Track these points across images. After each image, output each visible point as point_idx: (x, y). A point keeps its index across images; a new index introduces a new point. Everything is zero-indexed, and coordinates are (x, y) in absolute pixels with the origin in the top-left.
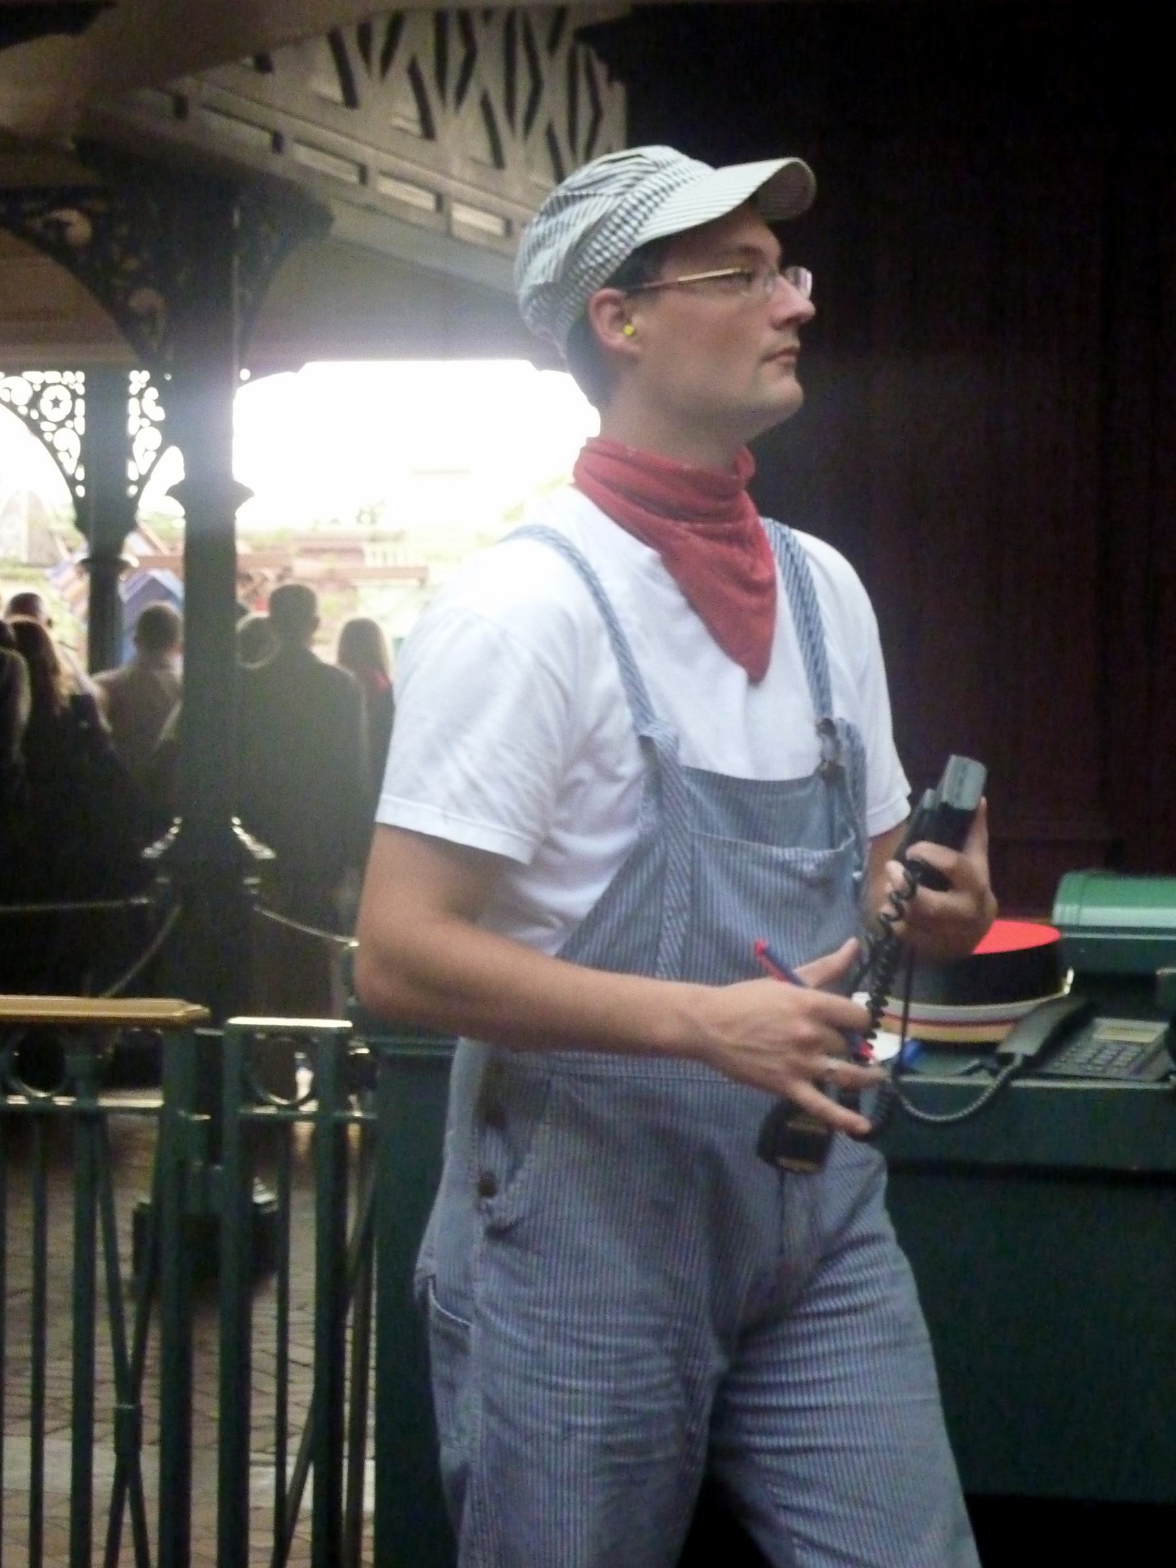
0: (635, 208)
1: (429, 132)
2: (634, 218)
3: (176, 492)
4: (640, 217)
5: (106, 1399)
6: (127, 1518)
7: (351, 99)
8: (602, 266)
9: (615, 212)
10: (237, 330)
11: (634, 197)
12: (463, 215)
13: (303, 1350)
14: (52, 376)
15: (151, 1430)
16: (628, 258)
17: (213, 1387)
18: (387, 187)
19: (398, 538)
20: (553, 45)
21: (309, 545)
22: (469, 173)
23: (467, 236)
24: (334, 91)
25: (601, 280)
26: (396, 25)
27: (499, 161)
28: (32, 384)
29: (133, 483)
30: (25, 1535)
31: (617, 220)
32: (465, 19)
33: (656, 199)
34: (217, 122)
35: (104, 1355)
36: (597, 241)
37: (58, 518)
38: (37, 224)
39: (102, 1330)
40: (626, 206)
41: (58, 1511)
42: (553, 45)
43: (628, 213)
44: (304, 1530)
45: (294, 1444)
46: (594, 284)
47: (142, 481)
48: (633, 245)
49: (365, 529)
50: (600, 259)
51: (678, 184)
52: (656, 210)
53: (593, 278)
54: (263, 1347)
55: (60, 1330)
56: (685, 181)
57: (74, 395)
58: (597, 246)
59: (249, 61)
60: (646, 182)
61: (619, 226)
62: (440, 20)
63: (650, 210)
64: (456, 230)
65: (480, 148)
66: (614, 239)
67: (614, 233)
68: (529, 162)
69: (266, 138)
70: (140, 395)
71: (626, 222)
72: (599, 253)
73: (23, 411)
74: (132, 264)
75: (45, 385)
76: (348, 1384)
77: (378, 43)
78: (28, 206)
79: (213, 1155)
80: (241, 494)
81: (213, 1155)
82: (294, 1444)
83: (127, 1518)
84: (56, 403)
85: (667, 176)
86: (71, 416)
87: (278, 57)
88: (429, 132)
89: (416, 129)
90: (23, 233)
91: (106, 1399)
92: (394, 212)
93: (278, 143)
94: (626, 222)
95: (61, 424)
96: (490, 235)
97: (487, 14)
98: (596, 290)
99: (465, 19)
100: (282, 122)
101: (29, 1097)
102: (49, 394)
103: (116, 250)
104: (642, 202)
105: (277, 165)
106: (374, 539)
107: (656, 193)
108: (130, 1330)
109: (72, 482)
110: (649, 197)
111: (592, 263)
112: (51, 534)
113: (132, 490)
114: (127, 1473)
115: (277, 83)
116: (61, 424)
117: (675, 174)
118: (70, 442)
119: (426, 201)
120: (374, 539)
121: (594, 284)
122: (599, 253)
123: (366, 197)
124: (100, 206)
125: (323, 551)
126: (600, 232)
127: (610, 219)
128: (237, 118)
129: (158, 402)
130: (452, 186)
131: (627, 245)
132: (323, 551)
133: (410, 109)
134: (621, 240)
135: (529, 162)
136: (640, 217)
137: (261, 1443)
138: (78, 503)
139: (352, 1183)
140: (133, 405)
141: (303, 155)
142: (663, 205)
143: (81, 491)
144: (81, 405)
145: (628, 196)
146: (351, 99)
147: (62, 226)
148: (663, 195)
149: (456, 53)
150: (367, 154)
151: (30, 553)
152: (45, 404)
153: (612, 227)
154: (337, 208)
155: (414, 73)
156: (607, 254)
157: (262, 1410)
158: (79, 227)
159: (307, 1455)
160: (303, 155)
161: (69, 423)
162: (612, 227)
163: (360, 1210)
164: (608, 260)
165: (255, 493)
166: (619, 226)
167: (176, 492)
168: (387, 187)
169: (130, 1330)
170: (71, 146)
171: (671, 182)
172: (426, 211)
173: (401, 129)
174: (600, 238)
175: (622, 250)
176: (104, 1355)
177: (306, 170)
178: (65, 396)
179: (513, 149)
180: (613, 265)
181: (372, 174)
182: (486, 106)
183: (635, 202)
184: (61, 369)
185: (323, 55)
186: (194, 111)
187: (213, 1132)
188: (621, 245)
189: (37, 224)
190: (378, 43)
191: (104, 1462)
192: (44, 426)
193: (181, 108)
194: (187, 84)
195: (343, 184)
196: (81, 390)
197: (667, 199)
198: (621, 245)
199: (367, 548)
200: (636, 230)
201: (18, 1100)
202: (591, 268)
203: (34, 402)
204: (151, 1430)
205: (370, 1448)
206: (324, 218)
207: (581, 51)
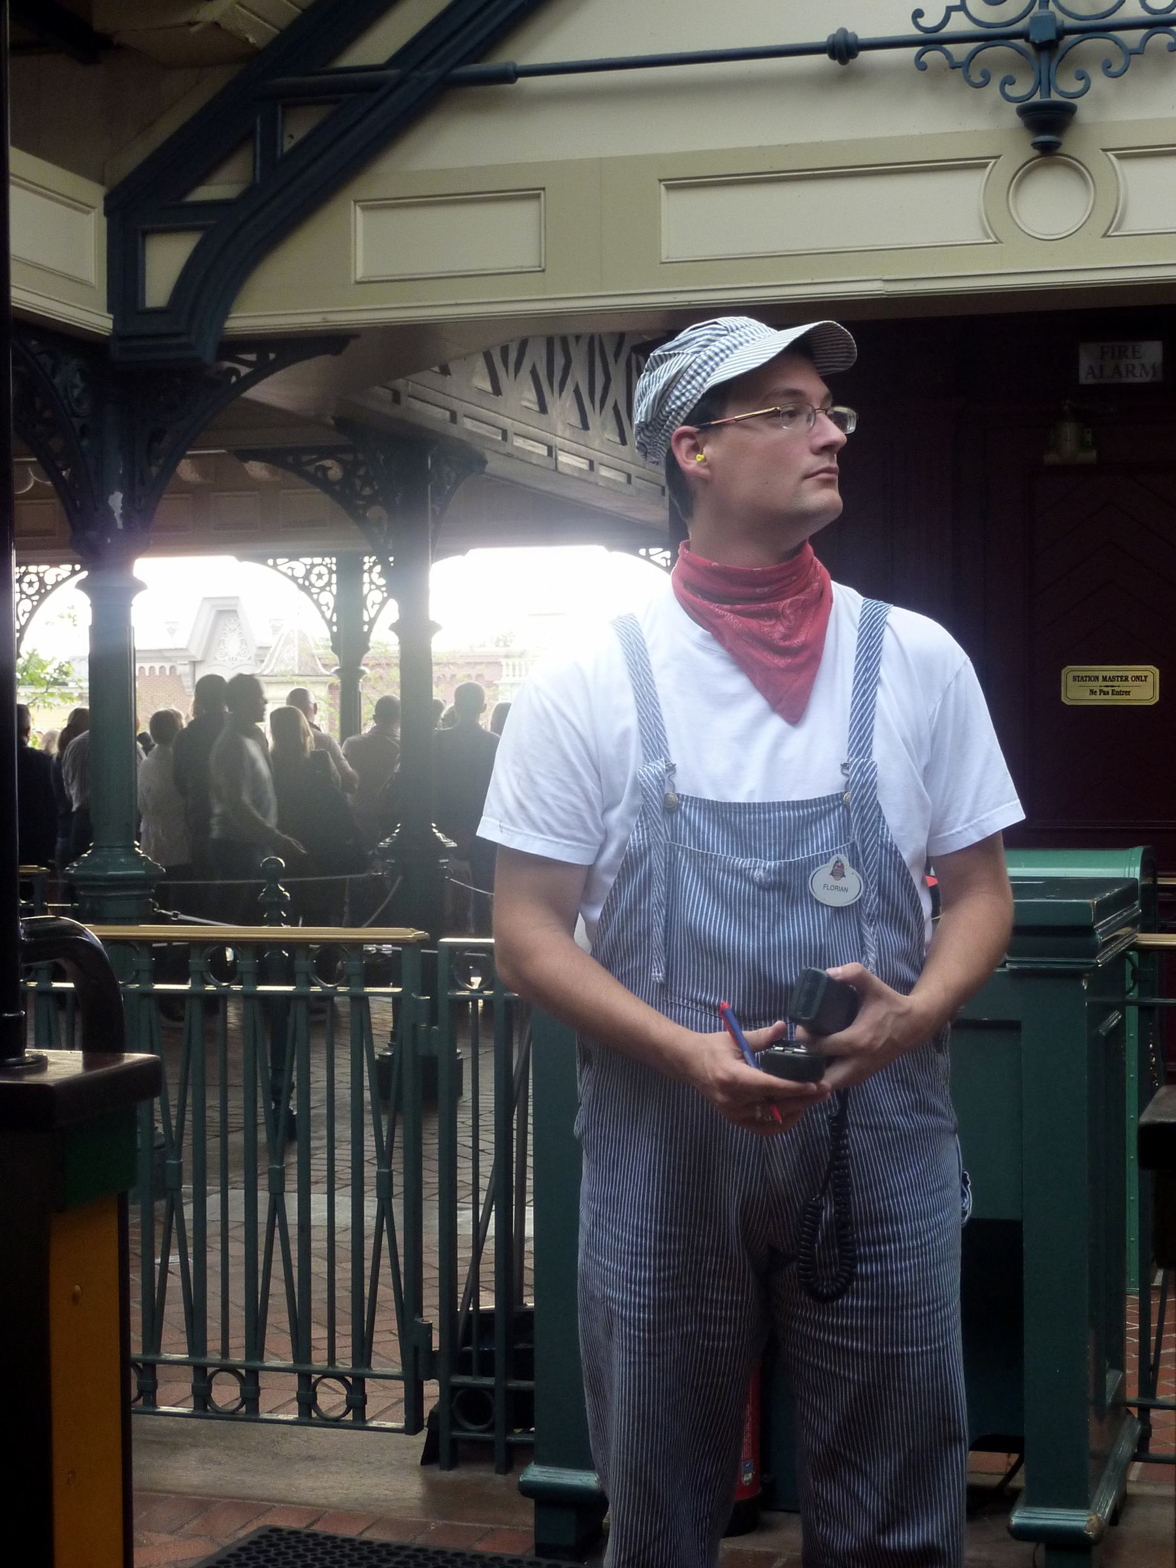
0: (706, 363)
1: (543, 409)
2: (705, 370)
3: (395, 628)
4: (708, 369)
5: (370, 1172)
6: (385, 1241)
7: (497, 391)
8: (681, 408)
9: (690, 366)
10: (431, 527)
11: (705, 354)
12: (563, 458)
13: (488, 1141)
14: (317, 560)
15: (398, 1189)
16: (700, 401)
17: (435, 1165)
18: (519, 442)
19: (522, 655)
20: (617, 355)
21: (468, 660)
22: (567, 434)
23: (567, 471)
24: (488, 387)
25: (682, 420)
26: (523, 345)
27: (585, 426)
28: (306, 565)
29: (366, 623)
30: (325, 1253)
31: (691, 373)
32: (564, 340)
33: (722, 355)
34: (418, 405)
35: (370, 1144)
36: (678, 389)
37: (317, 646)
38: (311, 469)
39: (369, 1133)
40: (699, 361)
41: (344, 1239)
42: (617, 355)
43: (700, 367)
44: (489, 1247)
45: (483, 1196)
46: (676, 422)
47: (372, 622)
48: (703, 391)
49: (502, 650)
50: (679, 403)
51: (741, 344)
52: (726, 360)
53: (675, 418)
54: (464, 1139)
55: (344, 1130)
56: (747, 342)
57: (331, 572)
58: (677, 393)
59: (436, 369)
60: (717, 343)
61: (693, 377)
62: (550, 341)
63: (722, 360)
64: (560, 468)
65: (575, 419)
66: (689, 387)
67: (689, 383)
68: (604, 427)
69: (448, 414)
70: (371, 569)
71: (699, 374)
72: (678, 398)
73: (301, 581)
74: (367, 491)
75: (313, 566)
76: (515, 1154)
77: (513, 356)
78: (305, 458)
79: (433, 1020)
80: (434, 628)
81: (433, 1020)
82: (483, 1196)
83: (385, 1241)
84: (320, 576)
85: (734, 337)
86: (329, 584)
87: (452, 367)
88: (543, 409)
89: (536, 407)
90: (303, 474)
91: (370, 1172)
92: (522, 458)
93: (454, 417)
94: (699, 374)
95: (322, 589)
96: (580, 469)
97: (578, 338)
98: (677, 426)
99: (564, 340)
100: (456, 405)
101: (322, 987)
102: (316, 570)
103: (358, 482)
104: (711, 358)
105: (454, 431)
106: (507, 656)
107: (722, 351)
108: (385, 1129)
109: (330, 623)
110: (717, 354)
111: (673, 407)
112: (313, 656)
113: (366, 628)
114: (385, 1211)
115: (452, 383)
116: (322, 589)
117: (741, 336)
118: (328, 598)
119: (543, 451)
120: (507, 656)
121: (676, 422)
122: (678, 398)
123: (508, 449)
124: (349, 457)
125: (276, 683)
126: (679, 382)
127: (686, 371)
128: (427, 402)
129: (381, 574)
130: (558, 441)
131: (699, 391)
132: (276, 683)
133: (532, 395)
134: (694, 388)
135: (604, 427)
136: (708, 369)
137: (464, 1196)
138: (334, 637)
139: (516, 1039)
140: (366, 577)
141: (469, 424)
142: (726, 360)
143: (335, 629)
144: (334, 577)
145: (702, 353)
146: (497, 391)
147: (325, 469)
148: (728, 352)
149: (559, 361)
150: (507, 423)
151: (299, 669)
152: (313, 578)
153: (688, 378)
154: (489, 456)
155: (534, 374)
156: (684, 399)
157: (464, 1175)
158: (335, 472)
159: (492, 1198)
160: (469, 424)
161: (328, 588)
162: (688, 378)
163: (520, 1052)
164: (684, 404)
165: (146, 583)
166: (693, 377)
167: (395, 628)
168: (519, 442)
169: (385, 1129)
170: (332, 422)
171: (736, 343)
172: (543, 456)
173: (526, 407)
174: (680, 387)
175: (695, 396)
176: (370, 1144)
177: (470, 433)
178: (324, 571)
179: (594, 419)
180: (688, 407)
181: (510, 434)
182: (577, 392)
183: (705, 358)
184: (323, 555)
185: (480, 364)
186: (404, 399)
187: (433, 1003)
188: (694, 392)
189: (311, 469)
190: (513, 356)
191: (371, 1208)
192: (314, 590)
193: (396, 397)
194: (400, 383)
195: (492, 440)
196: (334, 568)
197: (731, 356)
198: (694, 392)
199: (504, 662)
200: (705, 380)
201: (316, 989)
202: (673, 410)
203: (307, 577)
204: (398, 1189)
205: (529, 1197)
206: (483, 462)
207: (634, 357)
